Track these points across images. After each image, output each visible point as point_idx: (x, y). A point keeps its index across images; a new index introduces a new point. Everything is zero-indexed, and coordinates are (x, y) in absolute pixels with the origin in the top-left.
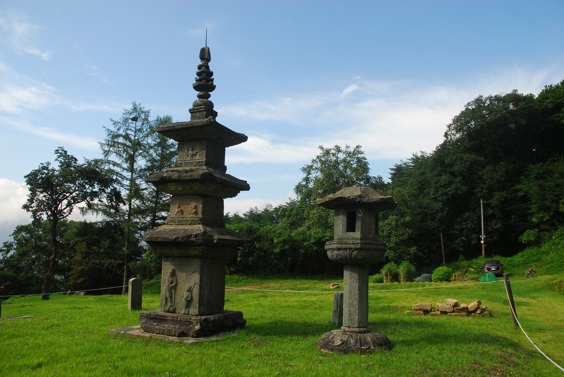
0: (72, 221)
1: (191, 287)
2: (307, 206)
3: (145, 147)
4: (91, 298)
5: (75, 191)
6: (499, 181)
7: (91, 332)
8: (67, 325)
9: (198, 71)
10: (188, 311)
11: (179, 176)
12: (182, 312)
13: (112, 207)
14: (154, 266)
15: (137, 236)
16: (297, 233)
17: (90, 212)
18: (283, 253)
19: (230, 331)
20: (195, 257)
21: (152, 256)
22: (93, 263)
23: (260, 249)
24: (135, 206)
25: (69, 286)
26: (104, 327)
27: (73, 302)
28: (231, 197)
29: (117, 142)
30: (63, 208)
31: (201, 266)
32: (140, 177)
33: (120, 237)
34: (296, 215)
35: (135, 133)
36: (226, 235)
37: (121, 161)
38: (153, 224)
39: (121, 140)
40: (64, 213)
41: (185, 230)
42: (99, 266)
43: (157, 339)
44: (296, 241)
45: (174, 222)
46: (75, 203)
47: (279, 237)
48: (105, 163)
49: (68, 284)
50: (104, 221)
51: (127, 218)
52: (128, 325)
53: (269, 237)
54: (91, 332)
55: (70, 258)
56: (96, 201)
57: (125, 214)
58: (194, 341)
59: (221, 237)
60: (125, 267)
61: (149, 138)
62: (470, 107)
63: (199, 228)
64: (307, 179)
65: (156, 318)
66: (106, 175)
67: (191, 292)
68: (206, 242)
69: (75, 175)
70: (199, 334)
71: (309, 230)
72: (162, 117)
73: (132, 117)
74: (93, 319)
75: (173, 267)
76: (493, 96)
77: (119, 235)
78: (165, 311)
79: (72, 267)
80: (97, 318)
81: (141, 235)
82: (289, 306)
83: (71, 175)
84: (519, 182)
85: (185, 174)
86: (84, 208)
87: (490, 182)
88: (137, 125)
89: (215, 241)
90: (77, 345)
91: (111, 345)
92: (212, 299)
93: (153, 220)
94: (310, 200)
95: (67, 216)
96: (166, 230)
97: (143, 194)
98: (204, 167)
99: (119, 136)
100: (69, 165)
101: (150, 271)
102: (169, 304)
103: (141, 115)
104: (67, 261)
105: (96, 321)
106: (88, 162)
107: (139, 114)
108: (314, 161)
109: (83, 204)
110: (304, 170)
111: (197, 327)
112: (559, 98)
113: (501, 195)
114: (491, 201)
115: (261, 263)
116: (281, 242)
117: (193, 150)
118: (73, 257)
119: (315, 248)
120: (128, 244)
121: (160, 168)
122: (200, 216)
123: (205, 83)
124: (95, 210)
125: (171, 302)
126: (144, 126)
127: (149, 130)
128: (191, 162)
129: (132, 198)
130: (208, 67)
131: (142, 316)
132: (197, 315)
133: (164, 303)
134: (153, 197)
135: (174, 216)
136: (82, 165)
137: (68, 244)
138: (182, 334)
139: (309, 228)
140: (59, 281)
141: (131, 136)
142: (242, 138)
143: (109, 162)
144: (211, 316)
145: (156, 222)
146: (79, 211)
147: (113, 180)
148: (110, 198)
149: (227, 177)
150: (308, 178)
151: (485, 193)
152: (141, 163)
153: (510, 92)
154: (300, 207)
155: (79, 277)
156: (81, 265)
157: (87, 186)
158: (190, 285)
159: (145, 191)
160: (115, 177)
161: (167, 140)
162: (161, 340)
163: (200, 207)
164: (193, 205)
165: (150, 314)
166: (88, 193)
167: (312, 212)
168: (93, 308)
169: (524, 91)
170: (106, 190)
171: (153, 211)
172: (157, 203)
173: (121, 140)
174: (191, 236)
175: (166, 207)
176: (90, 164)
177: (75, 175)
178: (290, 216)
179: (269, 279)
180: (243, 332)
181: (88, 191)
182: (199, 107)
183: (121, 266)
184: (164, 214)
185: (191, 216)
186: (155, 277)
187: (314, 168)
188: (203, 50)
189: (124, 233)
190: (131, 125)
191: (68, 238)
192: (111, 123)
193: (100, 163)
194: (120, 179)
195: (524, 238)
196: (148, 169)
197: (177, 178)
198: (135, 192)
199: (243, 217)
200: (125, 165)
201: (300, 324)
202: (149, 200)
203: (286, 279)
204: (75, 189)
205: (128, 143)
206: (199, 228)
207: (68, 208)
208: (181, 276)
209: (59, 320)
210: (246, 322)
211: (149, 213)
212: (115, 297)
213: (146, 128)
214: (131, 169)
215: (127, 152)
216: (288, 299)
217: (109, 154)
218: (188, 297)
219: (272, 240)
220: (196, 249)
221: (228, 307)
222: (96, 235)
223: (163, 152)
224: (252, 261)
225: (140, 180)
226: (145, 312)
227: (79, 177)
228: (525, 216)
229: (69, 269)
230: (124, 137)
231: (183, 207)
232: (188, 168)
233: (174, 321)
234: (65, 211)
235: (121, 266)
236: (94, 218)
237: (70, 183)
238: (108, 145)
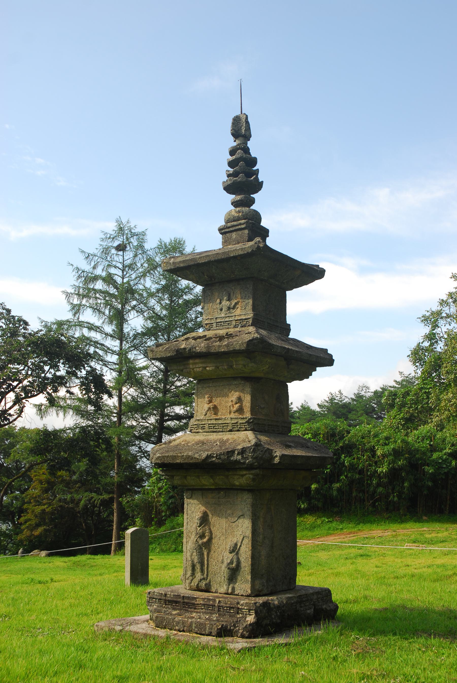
0: (23, 429)
1: (236, 544)
2: (435, 386)
3: (141, 295)
4: (59, 561)
5: (27, 376)
7: (64, 629)
8: (22, 615)
9: (231, 158)
10: (233, 589)
11: (208, 347)
12: (223, 589)
13: (89, 401)
14: (165, 503)
15: (133, 449)
16: (416, 436)
17: (53, 411)
18: (394, 474)
19: (310, 625)
20: (242, 489)
21: (160, 485)
22: (60, 500)
23: (352, 467)
24: (129, 398)
25: (21, 541)
26: (85, 618)
27: (29, 570)
28: (301, 379)
29: (93, 289)
30: (8, 406)
31: (254, 506)
32: (136, 347)
33: (105, 453)
34: (416, 404)
35: (123, 271)
36: (296, 447)
37: (101, 321)
38: (162, 429)
39: (99, 285)
40: (10, 415)
41: (223, 443)
42: (71, 505)
43: (179, 641)
44: (417, 450)
45: (203, 428)
46: (27, 397)
47: (386, 444)
48: (75, 326)
49: (19, 537)
50: (76, 426)
51: (115, 419)
52: (127, 613)
53: (367, 446)
54: (64, 629)
55: (22, 492)
56: (62, 392)
57: (112, 413)
58: (245, 645)
59: (288, 452)
60: (115, 506)
61: (148, 279)
63: (247, 438)
64: (431, 337)
65: (176, 602)
66: (77, 347)
67: (237, 554)
68: (260, 462)
69: (26, 350)
70: (255, 631)
71: (441, 430)
72: (167, 240)
73: (116, 244)
74: (67, 603)
75: (203, 508)
77: (103, 451)
78: (191, 589)
79: (25, 506)
80: (73, 601)
81: (140, 448)
82: (413, 576)
83: (19, 351)
85: (218, 343)
86: (41, 405)
88: (126, 258)
89: (277, 460)
90: (42, 652)
91: (100, 653)
92: (274, 564)
93: (161, 421)
94: (439, 376)
95: (15, 420)
96: (185, 442)
97: (142, 377)
98: (252, 329)
99: (95, 278)
100: (14, 333)
101: (159, 512)
102: (199, 576)
103: (132, 240)
104: (16, 498)
105: (71, 606)
106: (46, 326)
107: (127, 239)
108: (443, 303)
109: (41, 399)
110: (425, 319)
111: (251, 619)
115: (354, 494)
116: (390, 454)
117: (229, 299)
118: (26, 490)
119: (454, 463)
120: (119, 465)
121: (168, 330)
122: (248, 415)
123: (244, 179)
124: (61, 407)
125: (202, 571)
126: (137, 259)
127: (146, 265)
128: (226, 320)
129: (123, 385)
130: (246, 150)
131: (151, 598)
132: (248, 596)
133: (189, 573)
134: (159, 382)
135: (202, 417)
136: (37, 333)
137: (18, 469)
138: (224, 632)
139: (441, 427)
140: (5, 532)
141: (116, 278)
142: (313, 273)
143: (81, 324)
144: (275, 598)
145: (166, 424)
146: (35, 410)
147: (89, 354)
148: (85, 386)
149: (291, 344)
150: (434, 334)
152: (136, 323)
154: (421, 389)
155: (38, 525)
156: (40, 504)
157: (46, 368)
158: (235, 540)
159: (144, 372)
160: (92, 350)
161: (177, 281)
162: (187, 643)
163: (247, 400)
164: (234, 396)
165: (166, 595)
166: (48, 379)
167: (444, 396)
168: (64, 580)
170: (79, 373)
171: (160, 405)
172: (165, 391)
173: (99, 285)
174: (233, 452)
175: (184, 397)
176: (50, 330)
177: (26, 350)
178: (403, 405)
179: (371, 522)
180: (332, 627)
181: (49, 375)
182: (235, 223)
183: (107, 504)
184: (179, 410)
185: (233, 415)
186: (168, 524)
187: (444, 315)
188: (236, 121)
189: (112, 446)
190: (116, 258)
191: (17, 457)
192: (82, 257)
193: (66, 327)
194: (101, 352)
196: (149, 333)
197: (204, 350)
198: (129, 374)
199: (318, 409)
200: (109, 329)
201: (441, 614)
202: (152, 387)
203: (402, 522)
204: (27, 374)
205: (112, 290)
206: (247, 438)
207: (17, 407)
208: (218, 524)
209: (9, 605)
210: (337, 607)
211: (153, 409)
212: (99, 559)
213: (140, 261)
214: (120, 335)
215: (111, 305)
216: (409, 561)
217: (81, 311)
218: (231, 562)
219: (373, 451)
220: (243, 476)
221: (304, 579)
222: (65, 452)
223: (172, 301)
224: (339, 490)
225: (135, 352)
226: (156, 590)
227: (33, 352)
229: (21, 511)
230: (104, 280)
231: (216, 401)
232: (222, 332)
233: (209, 607)
234: (12, 412)
235: (107, 504)
236: (61, 421)
237: (19, 364)
238: (78, 295)
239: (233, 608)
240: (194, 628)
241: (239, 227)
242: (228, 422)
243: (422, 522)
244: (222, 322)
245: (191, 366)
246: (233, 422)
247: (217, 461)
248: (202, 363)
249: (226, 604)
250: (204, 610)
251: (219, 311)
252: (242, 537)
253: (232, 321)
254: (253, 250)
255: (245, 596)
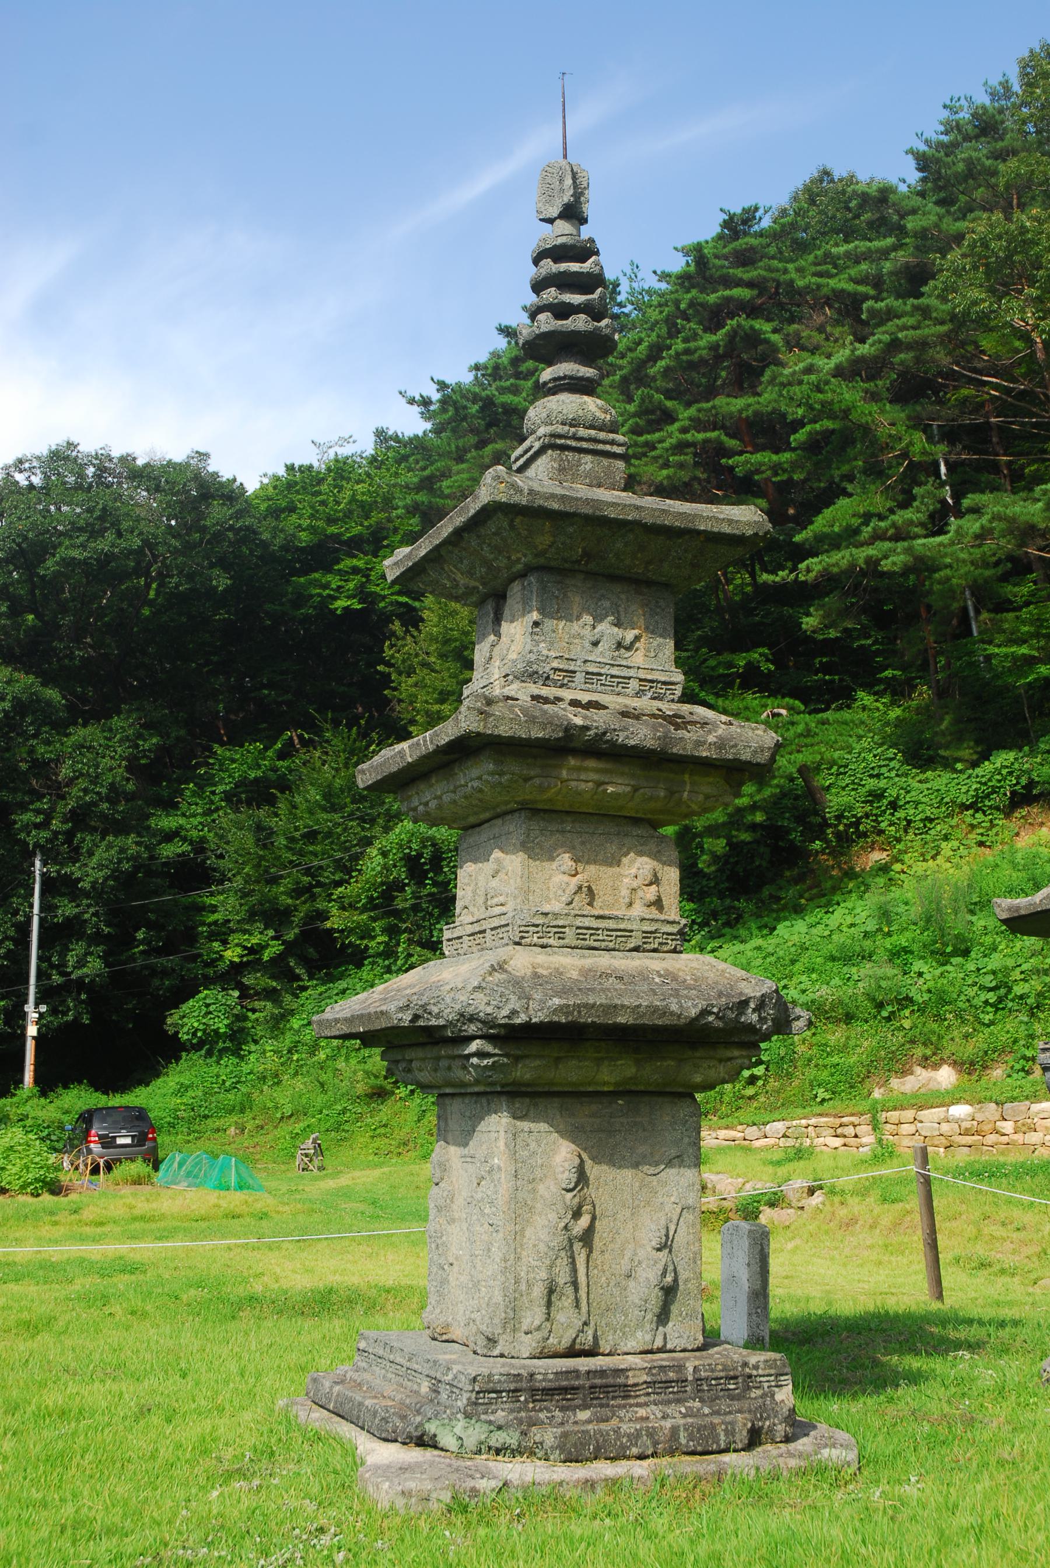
6: (115, 794)
62: (21, 478)
65: (565, 1390)
76: (116, 454)
84: (170, 805)
87: (86, 791)
112: (331, 521)
113: (122, 850)
114: (74, 870)
151: (56, 833)
153: (178, 455)
169: (224, 466)
174: (744, 1004)
182: (602, 435)
195: (190, 1018)
228: (182, 935)
239: (735, 1378)
240: (683, 1441)
241: (608, 447)
242: (634, 927)
243: (636, 1165)
244: (600, 674)
245: (564, 774)
246: (645, 928)
247: (720, 1024)
248: (597, 771)
249: (712, 1371)
250: (653, 1397)
251: (587, 645)
252: (679, 1210)
253: (629, 678)
254: (756, 534)
255: (693, 1350)
